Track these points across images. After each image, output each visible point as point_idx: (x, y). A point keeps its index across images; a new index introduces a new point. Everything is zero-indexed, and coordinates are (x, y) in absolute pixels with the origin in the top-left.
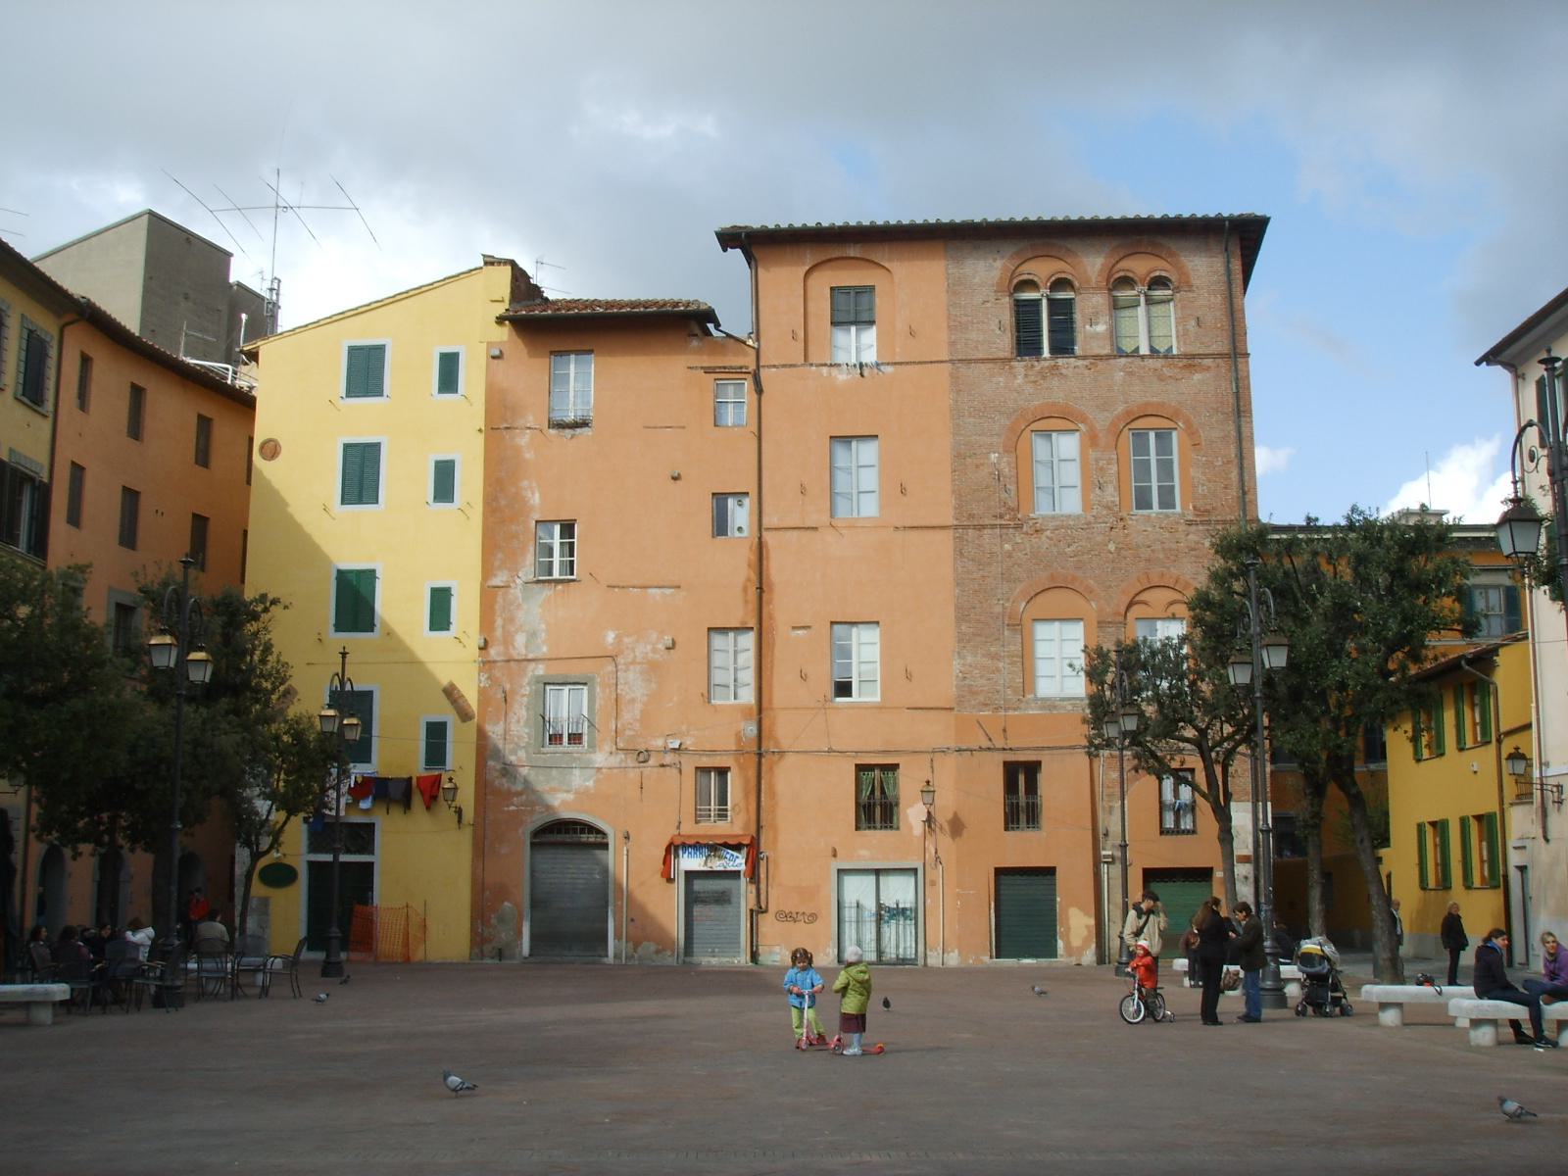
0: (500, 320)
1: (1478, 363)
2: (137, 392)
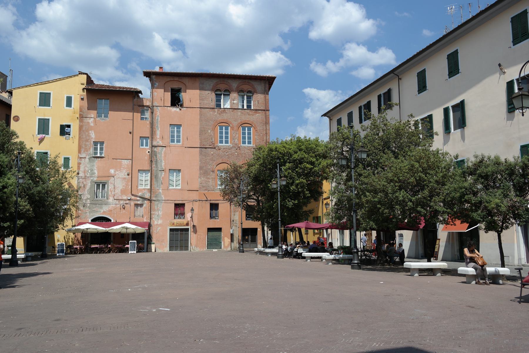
1: (322, 116)
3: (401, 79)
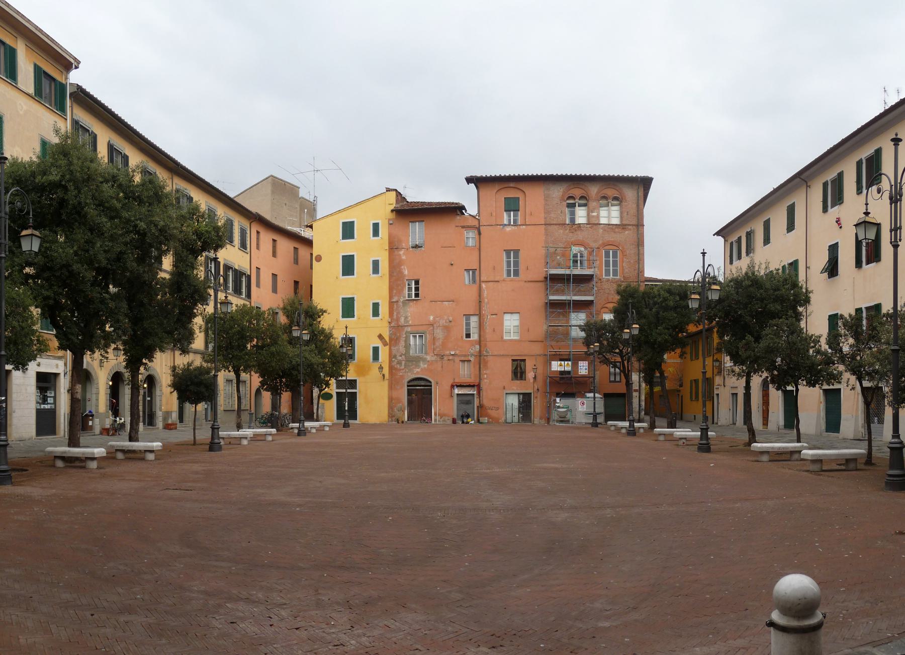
0: (392, 211)
1: (714, 235)
2: (274, 241)
3: (809, 186)
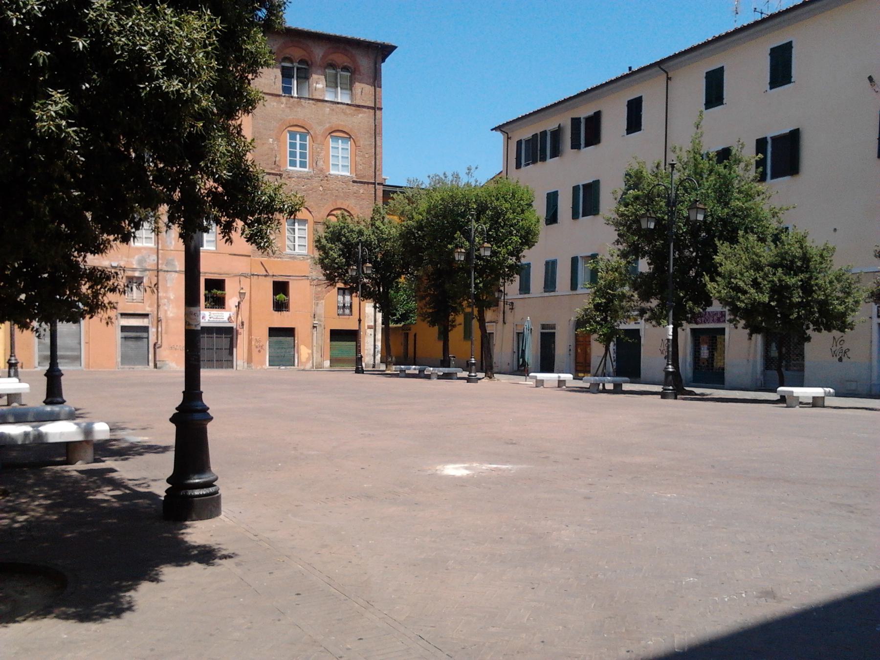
1: (492, 130)
